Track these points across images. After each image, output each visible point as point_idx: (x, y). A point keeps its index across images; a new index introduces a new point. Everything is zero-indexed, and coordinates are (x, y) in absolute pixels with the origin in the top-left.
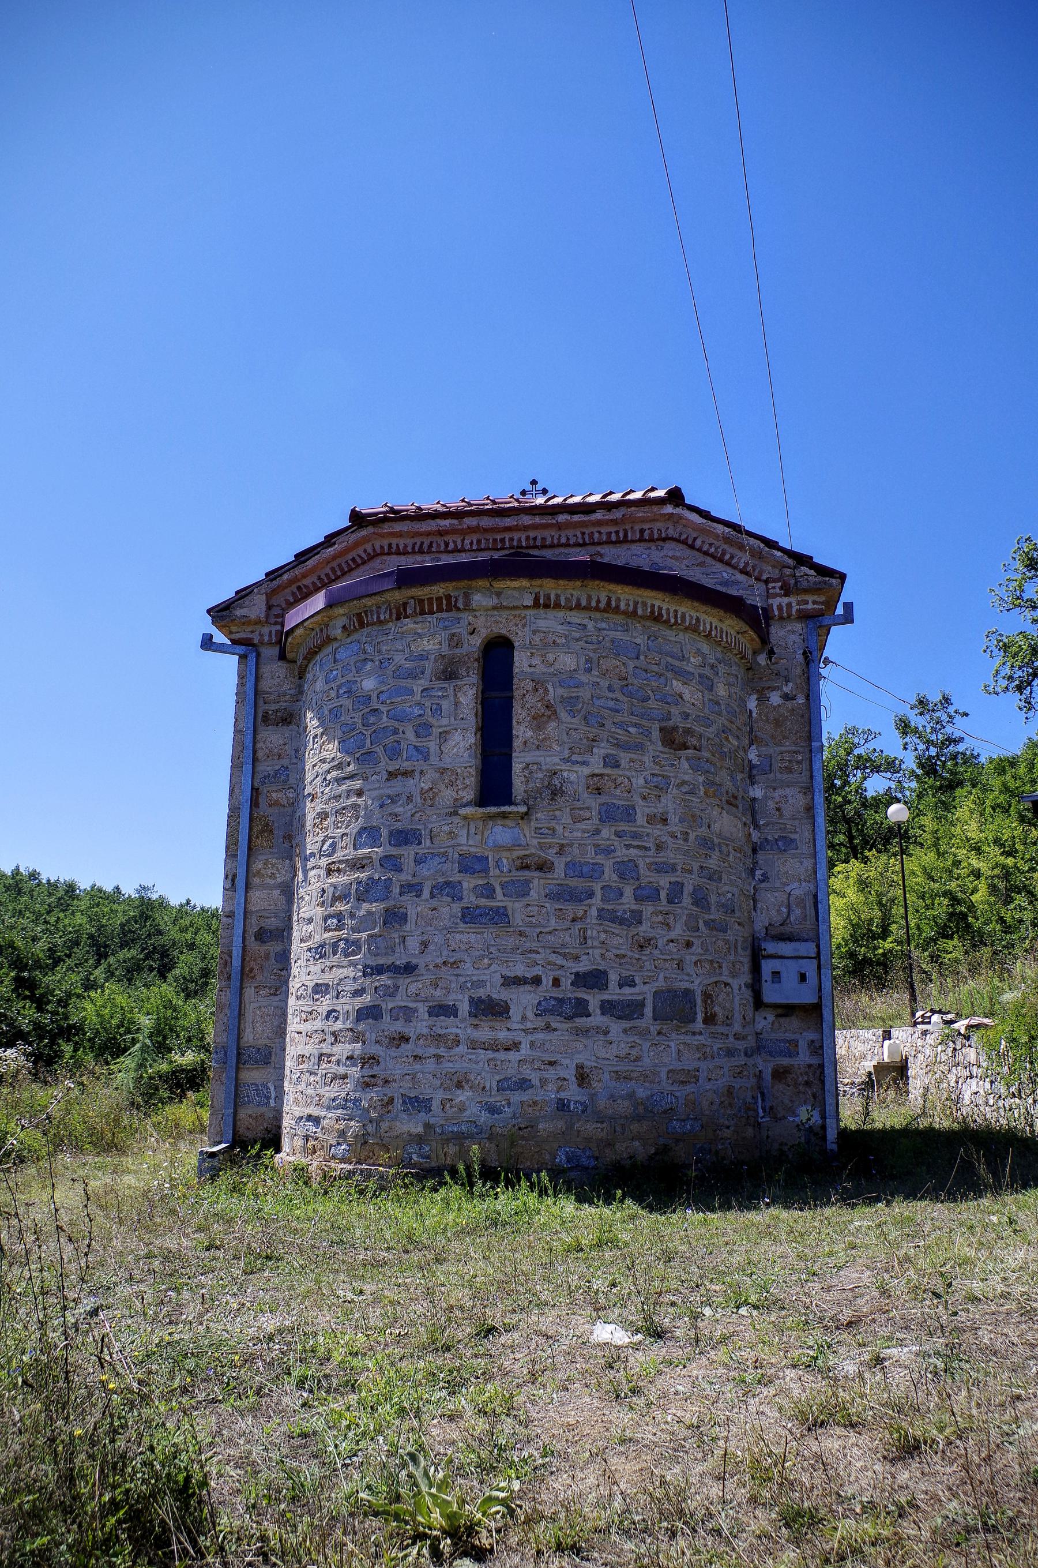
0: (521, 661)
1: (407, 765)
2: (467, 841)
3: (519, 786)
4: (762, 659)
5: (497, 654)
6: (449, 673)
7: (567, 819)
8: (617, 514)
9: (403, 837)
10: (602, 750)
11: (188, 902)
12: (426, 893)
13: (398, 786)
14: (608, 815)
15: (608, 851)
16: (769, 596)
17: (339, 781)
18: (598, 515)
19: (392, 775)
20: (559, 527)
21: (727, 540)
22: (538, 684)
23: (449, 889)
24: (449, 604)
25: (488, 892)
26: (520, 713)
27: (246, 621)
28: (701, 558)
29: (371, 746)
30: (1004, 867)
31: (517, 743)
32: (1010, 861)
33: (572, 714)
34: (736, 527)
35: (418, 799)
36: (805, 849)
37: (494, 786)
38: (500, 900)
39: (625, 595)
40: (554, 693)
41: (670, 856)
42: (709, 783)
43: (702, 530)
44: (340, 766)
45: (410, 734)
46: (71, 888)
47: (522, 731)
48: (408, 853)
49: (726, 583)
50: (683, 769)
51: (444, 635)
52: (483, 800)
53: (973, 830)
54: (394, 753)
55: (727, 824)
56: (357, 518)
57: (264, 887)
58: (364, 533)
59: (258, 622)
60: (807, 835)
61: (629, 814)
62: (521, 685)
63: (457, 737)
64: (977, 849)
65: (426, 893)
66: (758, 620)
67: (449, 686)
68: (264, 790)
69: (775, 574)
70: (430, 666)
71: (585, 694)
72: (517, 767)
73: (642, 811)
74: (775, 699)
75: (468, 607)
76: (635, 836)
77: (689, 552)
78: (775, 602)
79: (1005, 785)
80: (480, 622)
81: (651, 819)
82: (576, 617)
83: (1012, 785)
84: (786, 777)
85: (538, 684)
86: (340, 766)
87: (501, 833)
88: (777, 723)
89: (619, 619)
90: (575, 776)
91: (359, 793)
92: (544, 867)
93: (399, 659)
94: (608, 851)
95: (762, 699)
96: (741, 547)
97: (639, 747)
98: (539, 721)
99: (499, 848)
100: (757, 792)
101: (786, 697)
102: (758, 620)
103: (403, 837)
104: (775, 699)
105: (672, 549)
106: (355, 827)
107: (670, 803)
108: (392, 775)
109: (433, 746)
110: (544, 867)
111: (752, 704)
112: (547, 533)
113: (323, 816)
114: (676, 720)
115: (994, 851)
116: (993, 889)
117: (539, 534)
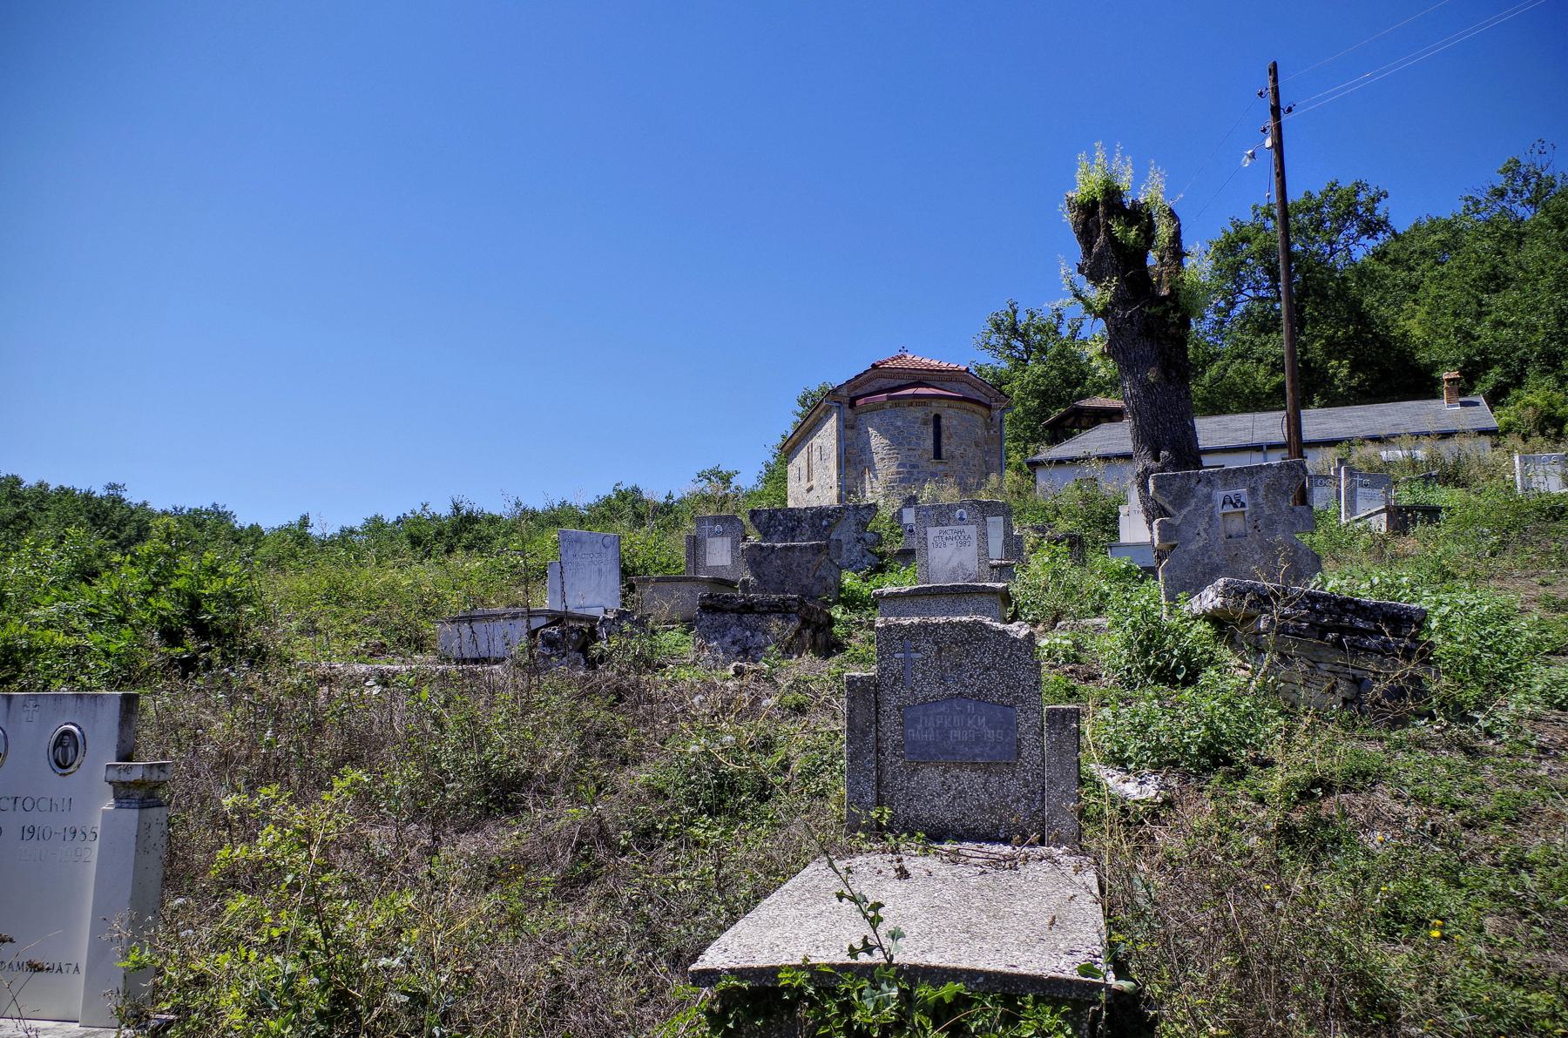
0: (944, 422)
3: (944, 454)
5: (937, 418)
6: (925, 423)
9: (913, 466)
29: (897, 440)
37: (938, 454)
39: (968, 405)
47: (944, 440)
62: (944, 428)
87: (941, 467)
90: (957, 453)
103: (913, 466)
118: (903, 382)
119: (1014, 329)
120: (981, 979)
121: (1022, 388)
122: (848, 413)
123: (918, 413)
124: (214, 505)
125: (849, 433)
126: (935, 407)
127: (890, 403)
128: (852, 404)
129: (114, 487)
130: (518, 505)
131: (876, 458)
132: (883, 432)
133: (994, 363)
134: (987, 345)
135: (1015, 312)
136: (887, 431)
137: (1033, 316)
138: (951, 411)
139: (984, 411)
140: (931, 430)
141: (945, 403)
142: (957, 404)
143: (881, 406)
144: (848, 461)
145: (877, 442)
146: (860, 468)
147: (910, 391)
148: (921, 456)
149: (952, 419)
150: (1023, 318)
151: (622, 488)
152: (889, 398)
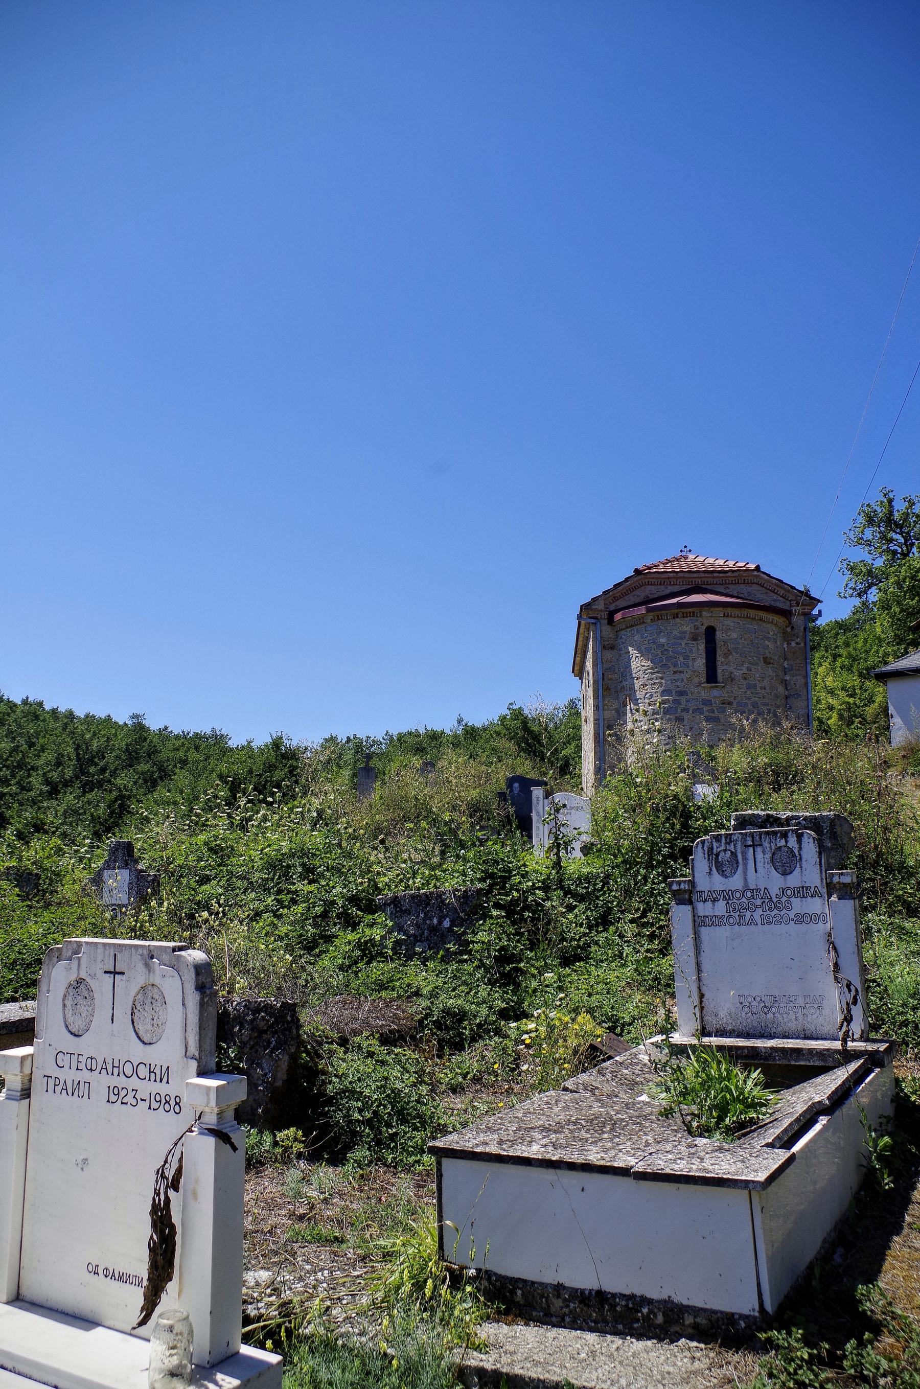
0: (719, 635)
1: (681, 669)
2: (704, 695)
3: (720, 677)
4: (789, 630)
5: (710, 632)
6: (695, 638)
7: (736, 688)
8: (736, 574)
9: (681, 693)
10: (746, 665)
11: (166, 728)
12: (691, 712)
13: (677, 676)
14: (749, 687)
15: (749, 698)
16: (791, 606)
17: (652, 673)
18: (729, 574)
19: (675, 672)
20: (714, 577)
21: (776, 585)
22: (725, 643)
23: (699, 710)
24: (693, 614)
25: (713, 712)
26: (719, 652)
27: (596, 610)
28: (765, 591)
29: (662, 661)
30: (848, 703)
31: (719, 663)
32: (851, 700)
33: (737, 653)
34: (781, 581)
35: (685, 680)
36: (805, 698)
37: (711, 676)
38: (716, 714)
39: (752, 613)
40: (730, 646)
41: (767, 700)
42: (777, 676)
43: (767, 581)
44: (652, 668)
45: (681, 659)
46: (70, 715)
47: (720, 659)
48: (683, 699)
49: (775, 601)
50: (770, 671)
51: (692, 625)
52: (708, 681)
53: (830, 681)
54: (675, 665)
55: (781, 689)
56: (636, 571)
57: (608, 710)
58: (640, 577)
59: (601, 611)
60: (805, 693)
61: (755, 686)
62: (719, 643)
63: (699, 660)
64: (831, 692)
65: (691, 712)
66: (786, 614)
67: (695, 643)
68: (606, 674)
69: (794, 598)
70: (687, 636)
71: (740, 646)
72: (719, 671)
73: (759, 685)
74: (793, 644)
75: (701, 616)
76: (757, 693)
77: (761, 588)
78: (794, 609)
79: (849, 653)
80: (705, 621)
81: (761, 688)
82: (736, 620)
83: (853, 653)
84: (798, 672)
85: (725, 643)
86: (652, 668)
87: (715, 693)
88: (794, 653)
89: (749, 620)
90: (738, 674)
91: (662, 678)
92: (730, 703)
93: (675, 632)
94: (749, 698)
95: (789, 644)
96: (781, 588)
97: (756, 664)
98: (726, 656)
99: (715, 697)
100: (787, 678)
101: (797, 643)
102: (786, 614)
103: (681, 693)
104: (793, 644)
105: (755, 587)
106: (661, 689)
107: (766, 683)
108: (675, 672)
109: (690, 663)
110: (730, 703)
111: (785, 646)
112: (709, 580)
113: (644, 685)
114: (767, 655)
115: (842, 694)
116: (841, 717)
117: (709, 580)
118: (676, 589)
119: (889, 520)
120: (888, 1183)
121: (899, 584)
122: (607, 630)
123: (686, 626)
124: (213, 730)
125: (609, 654)
126: (707, 618)
127: (650, 616)
128: (611, 621)
129: (135, 716)
130: (459, 721)
131: (637, 685)
132: (644, 653)
133: (868, 559)
134: (860, 541)
135: (890, 501)
136: (648, 650)
137: (912, 504)
138: (729, 622)
139: (779, 620)
140: (702, 647)
141: (719, 612)
142: (736, 612)
143: (641, 620)
144: (607, 689)
145: (638, 664)
146: (622, 696)
147: (674, 601)
148: (690, 680)
149: (730, 631)
150: (900, 506)
151: (514, 707)
152: (649, 610)
